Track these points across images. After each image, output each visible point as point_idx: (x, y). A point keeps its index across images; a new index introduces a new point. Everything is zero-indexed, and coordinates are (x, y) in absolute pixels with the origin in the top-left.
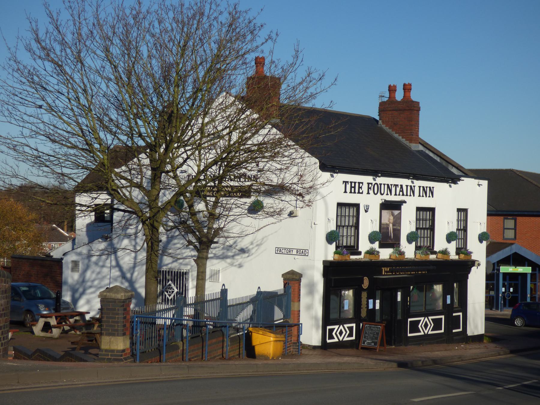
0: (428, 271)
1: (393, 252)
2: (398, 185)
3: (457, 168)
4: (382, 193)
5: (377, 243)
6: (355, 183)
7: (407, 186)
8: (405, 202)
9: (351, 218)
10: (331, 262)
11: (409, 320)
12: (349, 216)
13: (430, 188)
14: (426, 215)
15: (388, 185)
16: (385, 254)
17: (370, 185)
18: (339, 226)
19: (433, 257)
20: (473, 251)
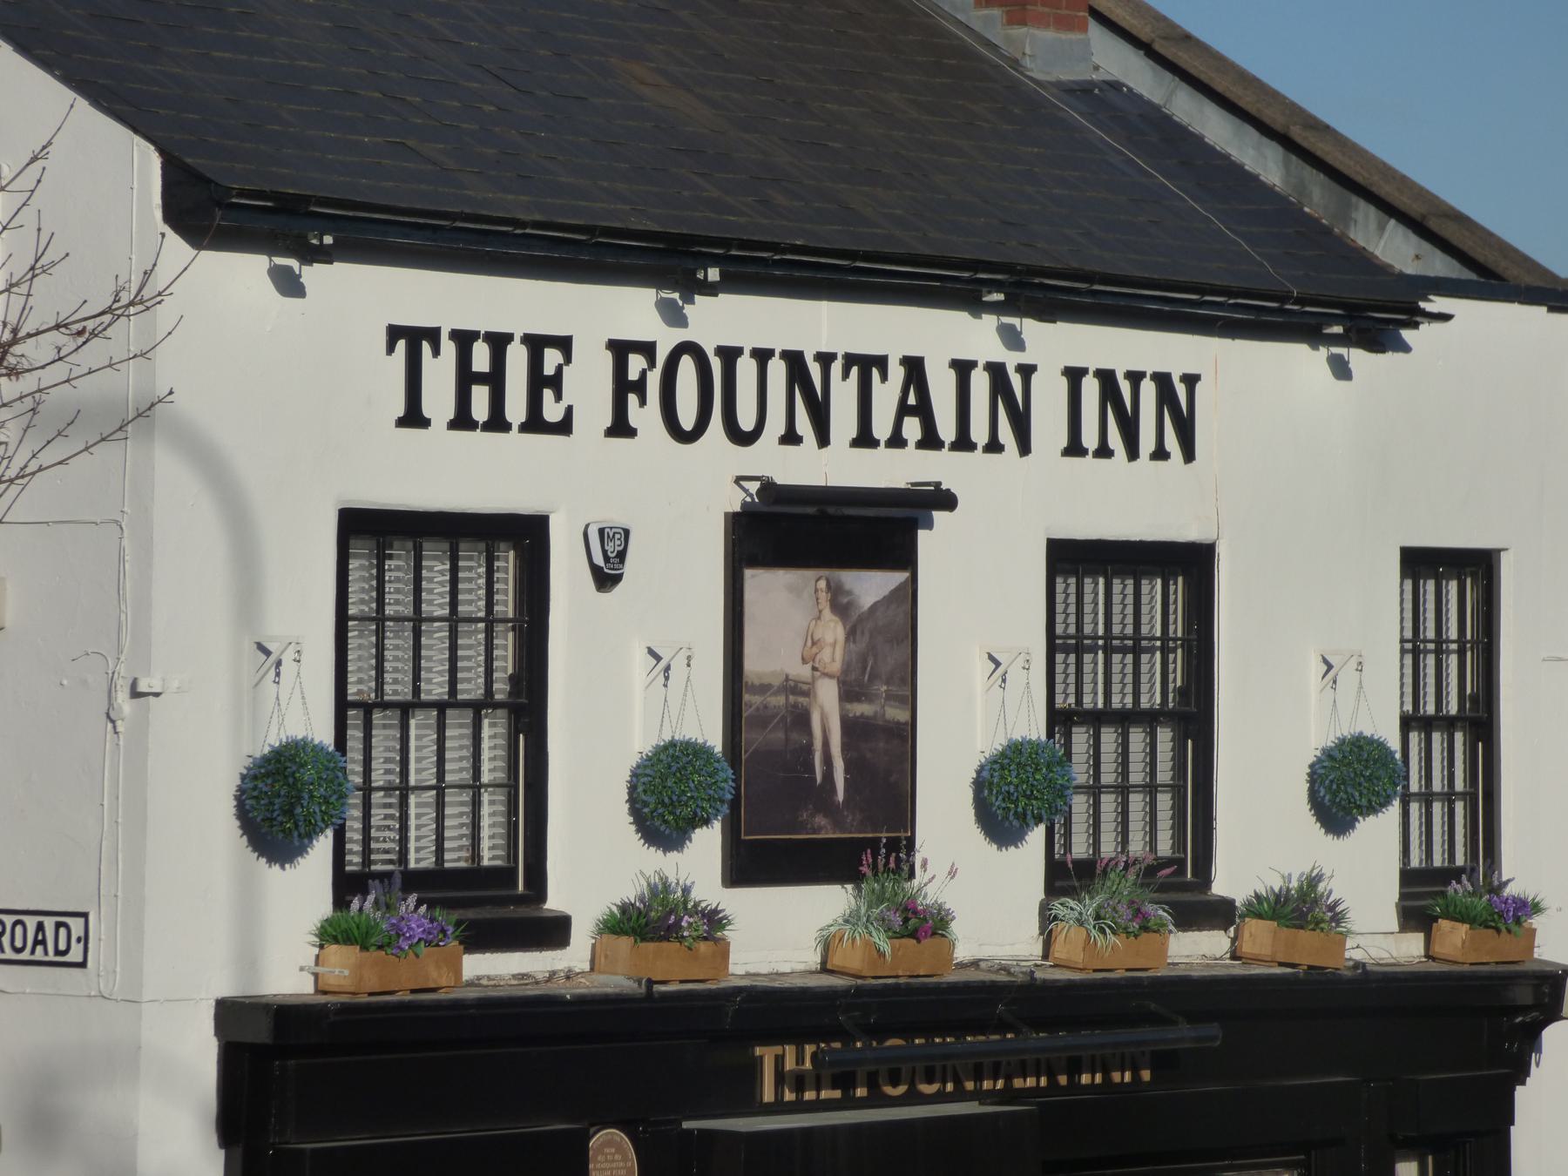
0: (1163, 1061)
1: (851, 919)
2: (881, 362)
3: (1418, 227)
4: (747, 422)
5: (708, 843)
6: (499, 342)
7: (963, 369)
8: (947, 501)
9: (472, 642)
10: (287, 1017)
12: (418, 620)
13: (1163, 380)
14: (1141, 612)
15: (794, 360)
16: (782, 933)
17: (636, 363)
18: (367, 709)
19: (1197, 950)
20: (1547, 898)
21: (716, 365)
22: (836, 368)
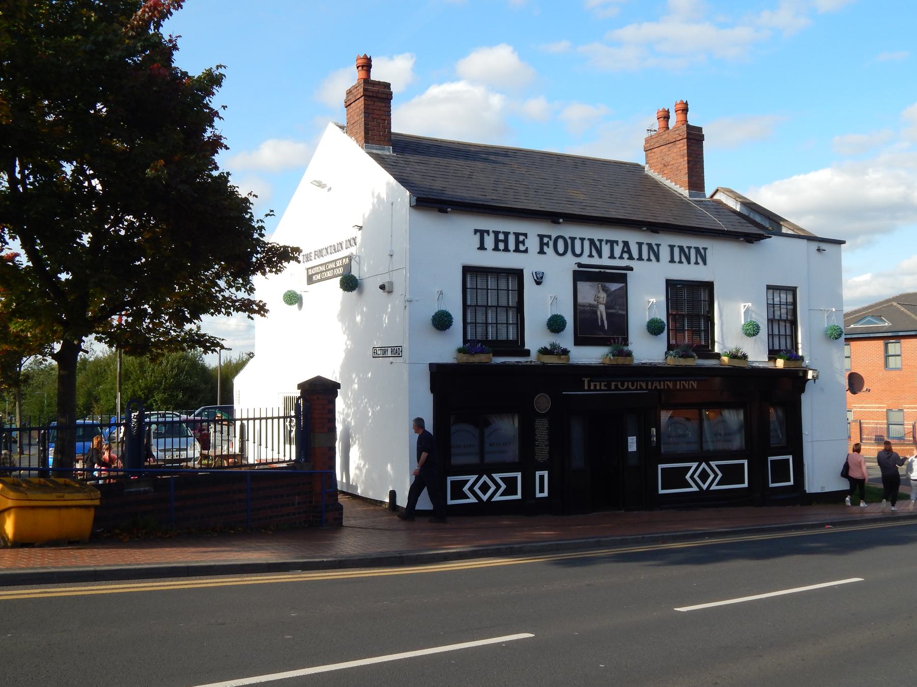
11: (770, 458)
16: (592, 355)
17: (546, 240)
21: (569, 241)
22: (603, 243)
